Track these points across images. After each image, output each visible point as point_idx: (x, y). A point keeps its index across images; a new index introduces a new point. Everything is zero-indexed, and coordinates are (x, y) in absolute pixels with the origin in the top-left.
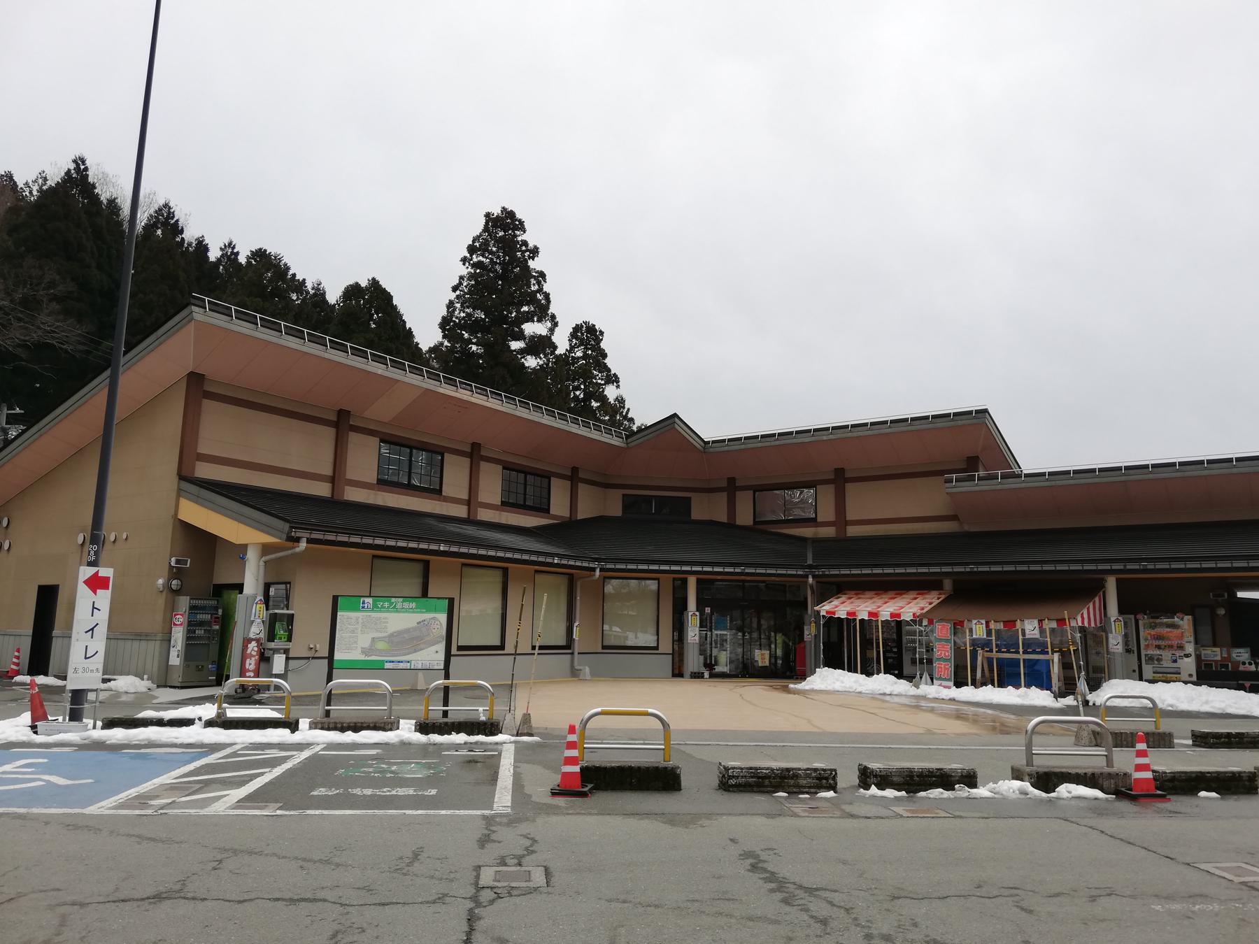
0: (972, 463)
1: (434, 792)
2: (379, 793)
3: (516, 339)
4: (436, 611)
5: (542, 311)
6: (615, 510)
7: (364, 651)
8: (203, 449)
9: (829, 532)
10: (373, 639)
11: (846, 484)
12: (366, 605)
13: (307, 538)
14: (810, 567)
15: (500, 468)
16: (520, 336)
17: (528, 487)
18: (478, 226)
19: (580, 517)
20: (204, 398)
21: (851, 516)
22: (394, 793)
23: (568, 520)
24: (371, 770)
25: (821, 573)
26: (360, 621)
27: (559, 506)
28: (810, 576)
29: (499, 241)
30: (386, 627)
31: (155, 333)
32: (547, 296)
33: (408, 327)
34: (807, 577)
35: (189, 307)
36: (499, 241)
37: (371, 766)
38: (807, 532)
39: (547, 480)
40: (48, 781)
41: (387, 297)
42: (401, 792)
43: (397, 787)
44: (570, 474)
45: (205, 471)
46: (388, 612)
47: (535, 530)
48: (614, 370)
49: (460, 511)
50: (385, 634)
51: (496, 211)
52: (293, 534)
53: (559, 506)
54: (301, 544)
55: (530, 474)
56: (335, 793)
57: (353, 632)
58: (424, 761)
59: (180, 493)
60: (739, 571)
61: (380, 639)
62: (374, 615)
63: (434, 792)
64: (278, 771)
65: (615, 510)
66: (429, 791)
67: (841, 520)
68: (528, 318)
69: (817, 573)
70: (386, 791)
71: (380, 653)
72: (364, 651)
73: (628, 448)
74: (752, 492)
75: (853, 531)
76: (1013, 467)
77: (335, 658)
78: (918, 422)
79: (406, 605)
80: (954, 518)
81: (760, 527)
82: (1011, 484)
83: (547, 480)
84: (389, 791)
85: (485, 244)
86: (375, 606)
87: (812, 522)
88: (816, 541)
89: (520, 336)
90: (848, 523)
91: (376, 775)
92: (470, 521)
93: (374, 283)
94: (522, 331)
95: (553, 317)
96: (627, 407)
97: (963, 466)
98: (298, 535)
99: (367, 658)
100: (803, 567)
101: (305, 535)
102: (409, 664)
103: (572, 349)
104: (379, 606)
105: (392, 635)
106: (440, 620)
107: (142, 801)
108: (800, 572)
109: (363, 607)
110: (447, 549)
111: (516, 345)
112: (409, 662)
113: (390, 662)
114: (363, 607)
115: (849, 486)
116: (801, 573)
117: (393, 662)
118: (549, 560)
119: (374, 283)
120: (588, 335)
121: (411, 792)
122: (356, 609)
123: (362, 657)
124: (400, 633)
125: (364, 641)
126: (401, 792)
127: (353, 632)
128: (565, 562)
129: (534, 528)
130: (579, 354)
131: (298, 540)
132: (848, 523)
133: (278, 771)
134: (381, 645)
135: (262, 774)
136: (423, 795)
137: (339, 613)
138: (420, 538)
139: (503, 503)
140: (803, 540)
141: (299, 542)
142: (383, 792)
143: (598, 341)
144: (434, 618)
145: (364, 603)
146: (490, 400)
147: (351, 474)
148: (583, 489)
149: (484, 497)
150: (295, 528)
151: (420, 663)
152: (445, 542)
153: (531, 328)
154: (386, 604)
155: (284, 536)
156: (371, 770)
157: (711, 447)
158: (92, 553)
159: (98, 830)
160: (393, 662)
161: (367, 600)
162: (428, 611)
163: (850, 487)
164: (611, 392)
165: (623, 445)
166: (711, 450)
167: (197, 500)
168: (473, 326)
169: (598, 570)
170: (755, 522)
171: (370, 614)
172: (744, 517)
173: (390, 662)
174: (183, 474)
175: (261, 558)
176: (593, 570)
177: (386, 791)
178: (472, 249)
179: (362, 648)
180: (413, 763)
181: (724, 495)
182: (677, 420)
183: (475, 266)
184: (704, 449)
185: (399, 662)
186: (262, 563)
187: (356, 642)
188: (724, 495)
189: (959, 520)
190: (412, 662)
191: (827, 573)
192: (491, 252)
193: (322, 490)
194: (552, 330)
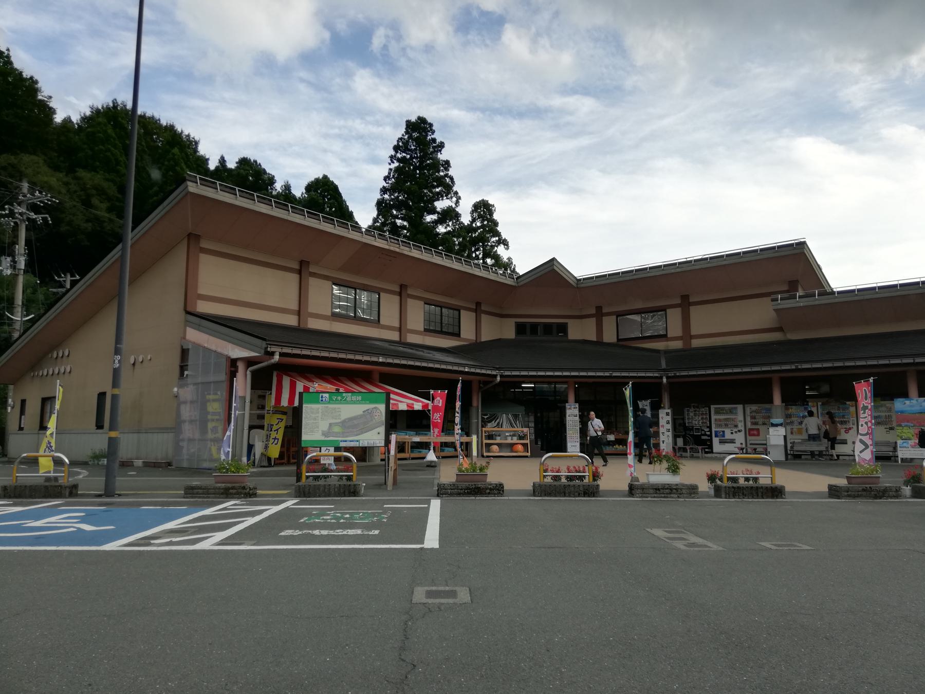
0: (793, 286)
1: (377, 532)
2: (334, 533)
3: (430, 213)
4: (376, 402)
5: (448, 188)
6: (509, 333)
7: (324, 434)
8: (201, 291)
9: (678, 345)
10: (331, 425)
11: (691, 307)
12: (324, 399)
13: (280, 353)
14: (664, 370)
15: (423, 303)
16: (433, 211)
17: (444, 317)
18: (401, 131)
19: (484, 339)
20: (201, 253)
21: (694, 331)
22: (345, 533)
23: (474, 342)
24: (328, 517)
25: (673, 374)
26: (320, 411)
27: (468, 333)
28: (664, 377)
29: (416, 140)
30: (340, 415)
31: (162, 205)
32: (452, 179)
33: (350, 210)
34: (661, 378)
35: (185, 183)
36: (416, 140)
37: (328, 515)
38: (660, 345)
39: (457, 312)
40: (79, 529)
41: (335, 189)
42: (351, 532)
43: (347, 529)
44: (475, 308)
45: (204, 307)
46: (341, 403)
47: (450, 350)
48: (504, 236)
49: (395, 336)
50: (339, 421)
51: (413, 119)
52: (269, 349)
53: (468, 333)
54: (275, 357)
55: (446, 307)
56: (298, 533)
57: (315, 419)
58: (369, 512)
59: (187, 323)
60: (608, 374)
61: (336, 424)
62: (330, 406)
63: (377, 532)
64: (257, 519)
65: (509, 333)
66: (373, 531)
67: (687, 335)
68: (439, 196)
69: (670, 375)
70: (339, 532)
71: (336, 434)
72: (324, 434)
73: (518, 286)
74: (615, 316)
75: (696, 343)
76: (825, 287)
77: (303, 439)
78: (748, 255)
79: (354, 398)
80: (780, 329)
81: (621, 343)
82: (825, 300)
83: (457, 312)
84: (340, 532)
85: (406, 144)
86: (331, 399)
87: (664, 337)
88: (667, 352)
89: (433, 211)
90: (692, 337)
91: (333, 521)
92: (400, 343)
93: (325, 177)
94: (435, 208)
95: (456, 193)
96: (514, 264)
97: (785, 288)
98: (273, 349)
99: (326, 439)
100: (658, 370)
101: (277, 350)
102: (358, 443)
103: (474, 220)
104: (334, 399)
105: (344, 421)
106: (380, 409)
107: (146, 541)
108: (656, 375)
109: (322, 401)
110: (384, 361)
111: (429, 218)
112: (358, 441)
113: (344, 441)
114: (322, 401)
115: (692, 308)
116: (657, 375)
117: (346, 441)
118: (461, 369)
119: (325, 177)
120: (483, 209)
121: (359, 532)
122: (317, 402)
123: (323, 438)
124: (351, 419)
125: (324, 426)
126: (351, 532)
127: (315, 419)
128: (473, 370)
129: (450, 348)
130: (479, 224)
131: (273, 354)
132: (692, 337)
133: (257, 519)
134: (337, 429)
135: (243, 521)
136: (368, 534)
137: (304, 405)
138: (363, 352)
139: (426, 330)
140: (657, 351)
141: (273, 355)
142: (337, 532)
143: (491, 214)
144: (375, 408)
145: (322, 397)
146: (413, 250)
147: (312, 309)
148: (484, 318)
149: (411, 325)
150: (270, 345)
151: (366, 442)
152: (383, 355)
153: (441, 205)
154: (339, 398)
155: (263, 351)
156: (328, 517)
157: (582, 283)
158: (117, 361)
159: (43, 538)
160: (346, 441)
161: (324, 395)
162: (371, 402)
163: (693, 310)
164: (500, 250)
165: (513, 284)
166: (583, 285)
167: (198, 328)
168: (399, 205)
169: (499, 376)
170: (618, 340)
171: (326, 405)
172: (610, 336)
173: (344, 441)
174: (189, 309)
175: (248, 368)
176: (495, 376)
177: (339, 532)
178: (396, 148)
179: (322, 431)
180: (361, 512)
181: (594, 320)
182: (555, 263)
183: (399, 160)
184: (577, 285)
185: (351, 441)
186: (248, 373)
187: (318, 427)
188: (594, 320)
189: (783, 331)
190: (361, 441)
191: (678, 374)
192: (411, 150)
193: (292, 321)
194: (457, 203)
